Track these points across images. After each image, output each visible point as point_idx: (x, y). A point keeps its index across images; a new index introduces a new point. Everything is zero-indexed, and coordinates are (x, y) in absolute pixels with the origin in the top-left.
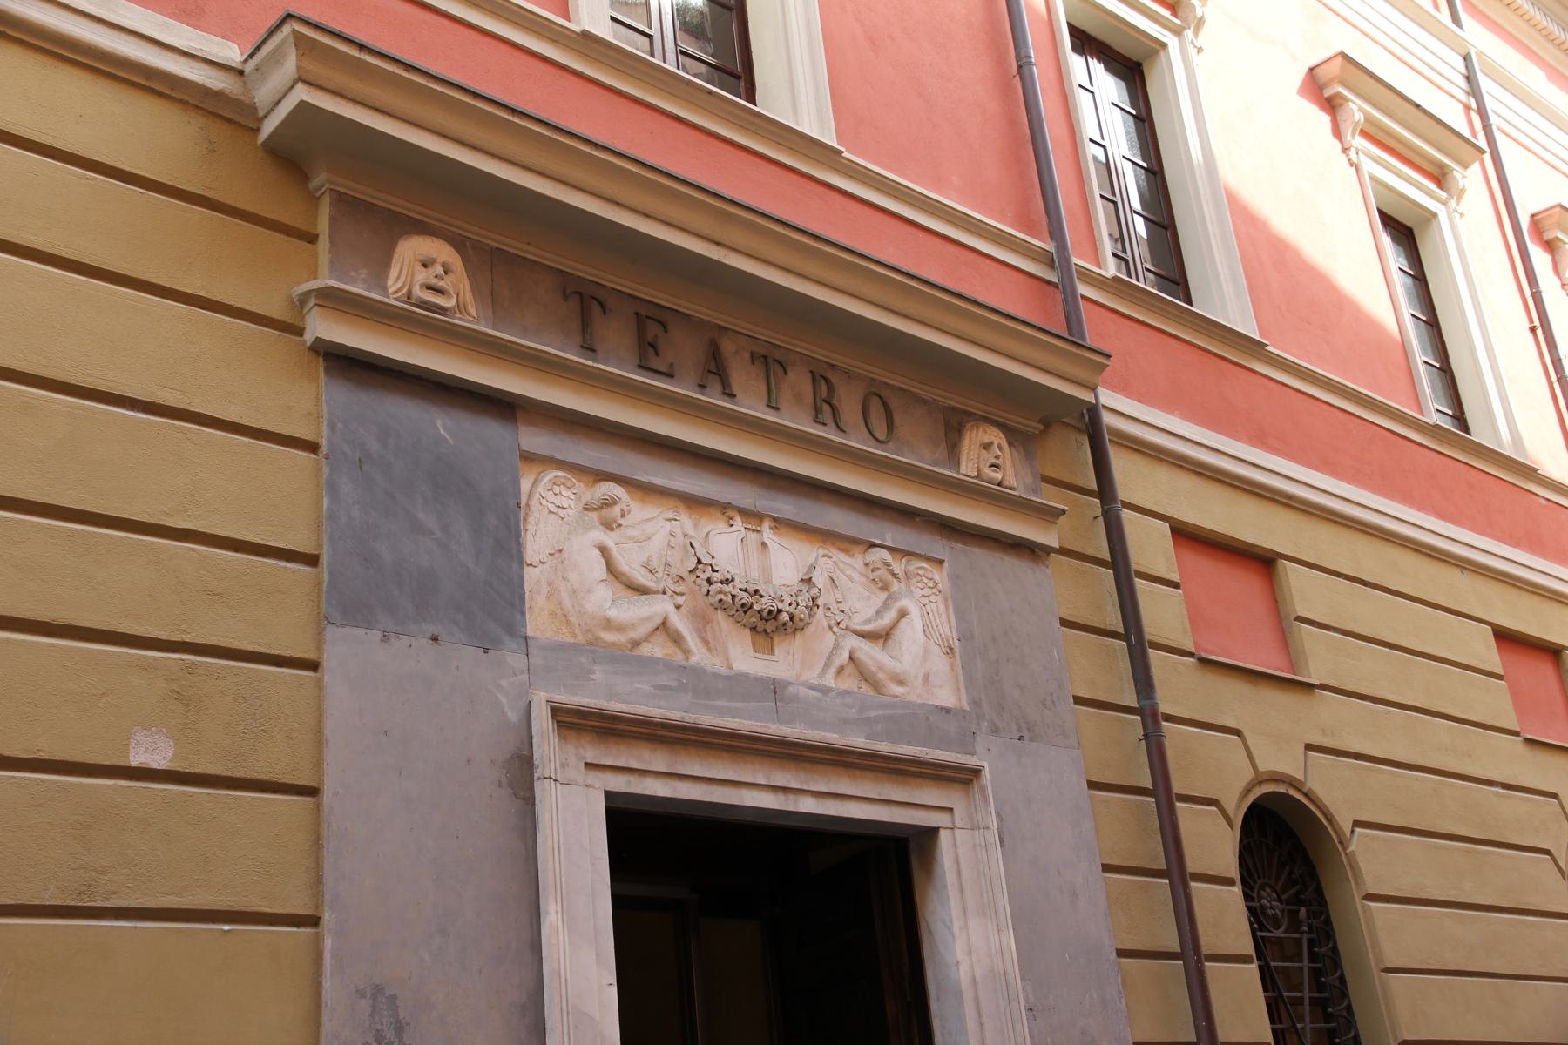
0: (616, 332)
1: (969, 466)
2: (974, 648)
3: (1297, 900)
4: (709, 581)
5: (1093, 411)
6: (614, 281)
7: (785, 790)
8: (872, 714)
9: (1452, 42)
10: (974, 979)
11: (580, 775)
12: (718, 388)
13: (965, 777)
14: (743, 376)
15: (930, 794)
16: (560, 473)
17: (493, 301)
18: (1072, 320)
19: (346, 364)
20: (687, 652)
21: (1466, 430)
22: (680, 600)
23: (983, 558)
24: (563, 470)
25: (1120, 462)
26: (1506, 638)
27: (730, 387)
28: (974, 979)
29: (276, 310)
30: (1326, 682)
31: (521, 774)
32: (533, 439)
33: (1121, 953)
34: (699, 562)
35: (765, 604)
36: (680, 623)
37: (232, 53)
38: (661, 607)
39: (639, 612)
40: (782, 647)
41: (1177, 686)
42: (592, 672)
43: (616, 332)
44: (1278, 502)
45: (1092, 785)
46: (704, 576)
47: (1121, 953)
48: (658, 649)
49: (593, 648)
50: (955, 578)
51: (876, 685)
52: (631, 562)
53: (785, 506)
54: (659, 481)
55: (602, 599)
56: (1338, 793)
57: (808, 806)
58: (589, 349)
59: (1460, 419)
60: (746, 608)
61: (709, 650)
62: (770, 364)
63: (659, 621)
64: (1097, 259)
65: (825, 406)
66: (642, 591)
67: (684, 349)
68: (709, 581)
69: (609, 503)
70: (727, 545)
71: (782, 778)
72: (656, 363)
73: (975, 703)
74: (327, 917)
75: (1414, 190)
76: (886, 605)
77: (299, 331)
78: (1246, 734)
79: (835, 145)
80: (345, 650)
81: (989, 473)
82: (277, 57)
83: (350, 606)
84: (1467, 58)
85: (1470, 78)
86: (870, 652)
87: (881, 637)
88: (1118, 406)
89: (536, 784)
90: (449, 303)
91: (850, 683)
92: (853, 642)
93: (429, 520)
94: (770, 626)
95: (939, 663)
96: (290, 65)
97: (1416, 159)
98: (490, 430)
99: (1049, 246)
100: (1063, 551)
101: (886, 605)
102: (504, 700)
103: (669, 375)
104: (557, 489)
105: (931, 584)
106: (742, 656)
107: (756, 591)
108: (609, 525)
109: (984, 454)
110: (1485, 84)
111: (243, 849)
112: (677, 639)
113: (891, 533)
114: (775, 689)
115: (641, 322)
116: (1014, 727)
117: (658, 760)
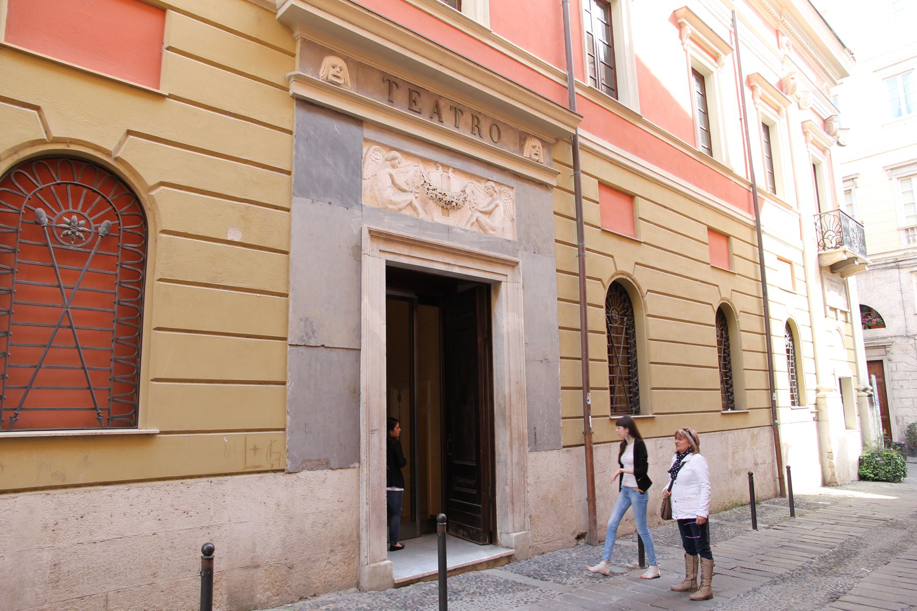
0: (401, 96)
2: (521, 220)
7: (449, 264)
11: (377, 253)
13: (513, 265)
14: (447, 115)
17: (357, 81)
18: (571, 102)
19: (304, 103)
20: (418, 214)
21: (711, 155)
32: (368, 133)
36: (416, 203)
38: (410, 197)
40: (453, 214)
41: (592, 238)
45: (558, 271)
48: (408, 212)
49: (384, 210)
50: (517, 194)
52: (400, 181)
54: (412, 152)
55: (390, 193)
56: (643, 280)
57: (457, 270)
58: (391, 101)
59: (710, 150)
62: (457, 111)
65: (476, 128)
66: (404, 191)
69: (394, 159)
70: (436, 177)
73: (520, 239)
76: (491, 203)
80: (299, 205)
83: (301, 190)
84: (733, 12)
86: (483, 218)
87: (488, 213)
88: (585, 135)
91: (475, 229)
92: (478, 214)
93: (329, 160)
94: (449, 207)
95: (508, 224)
98: (353, 129)
99: (566, 73)
101: (491, 203)
106: (437, 216)
108: (393, 167)
109: (533, 149)
111: (262, 270)
112: (415, 209)
113: (496, 176)
114: (448, 229)
115: (411, 92)
117: (405, 250)
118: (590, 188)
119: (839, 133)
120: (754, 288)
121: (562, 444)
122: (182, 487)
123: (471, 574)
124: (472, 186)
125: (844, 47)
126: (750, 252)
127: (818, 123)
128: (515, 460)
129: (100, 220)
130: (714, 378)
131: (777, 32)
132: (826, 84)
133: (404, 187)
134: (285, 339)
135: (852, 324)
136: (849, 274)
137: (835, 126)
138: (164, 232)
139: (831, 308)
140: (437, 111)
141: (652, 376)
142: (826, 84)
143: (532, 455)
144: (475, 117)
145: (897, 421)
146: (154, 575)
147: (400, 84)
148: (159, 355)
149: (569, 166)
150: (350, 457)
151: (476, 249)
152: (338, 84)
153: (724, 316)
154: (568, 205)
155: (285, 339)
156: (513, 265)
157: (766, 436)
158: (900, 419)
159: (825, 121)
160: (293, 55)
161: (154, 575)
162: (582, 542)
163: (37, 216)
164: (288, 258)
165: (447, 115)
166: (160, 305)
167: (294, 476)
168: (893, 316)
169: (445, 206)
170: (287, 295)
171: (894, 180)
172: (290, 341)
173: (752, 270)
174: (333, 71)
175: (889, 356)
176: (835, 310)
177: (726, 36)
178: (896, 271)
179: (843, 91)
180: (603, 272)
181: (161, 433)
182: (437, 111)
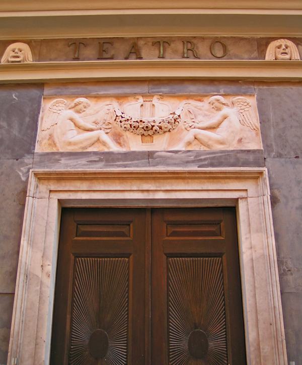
1: (269, 56)
4: (121, 122)
7: (148, 191)
8: (203, 157)
10: (252, 260)
12: (134, 56)
16: (55, 100)
20: (109, 148)
22: (108, 131)
24: (54, 98)
27: (140, 55)
28: (252, 260)
34: (117, 116)
42: (60, 160)
43: (90, 51)
46: (119, 121)
52: (82, 122)
53: (127, 89)
60: (136, 128)
61: (121, 146)
62: (161, 44)
63: (96, 139)
68: (121, 122)
70: (133, 109)
71: (146, 186)
72: (105, 56)
73: (267, 146)
81: (280, 56)
89: (27, 198)
94: (150, 132)
102: (21, 174)
103: (112, 58)
104: (57, 105)
105: (246, 104)
107: (141, 121)
112: (104, 144)
114: (150, 155)
116: (292, 153)
117: (84, 186)
164: (241, 198)
169: (146, 133)
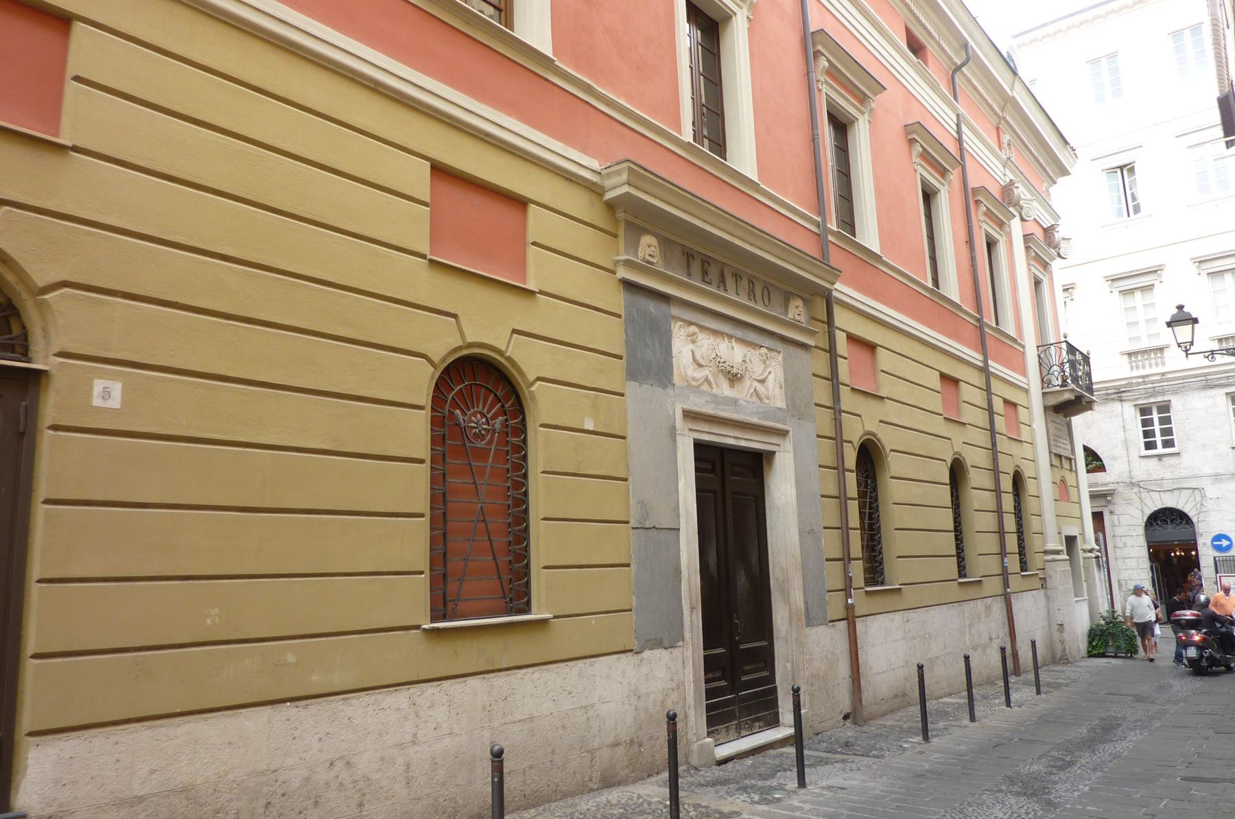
0: (696, 268)
2: (791, 385)
3: (867, 477)
5: (830, 291)
6: (715, 256)
9: (953, 108)
11: (687, 432)
13: (783, 434)
14: (730, 281)
15: (774, 440)
17: (666, 258)
18: (824, 252)
19: (628, 285)
21: (937, 287)
23: (793, 351)
25: (994, 382)
26: (440, 171)
29: (610, 267)
30: (81, 144)
31: (673, 431)
32: (675, 311)
33: (822, 496)
35: (735, 371)
36: (710, 378)
37: (595, 165)
38: (705, 372)
39: (700, 374)
40: (738, 386)
41: (848, 401)
44: (439, 120)
45: (818, 436)
47: (822, 496)
48: (705, 387)
49: (693, 388)
50: (784, 358)
51: (761, 399)
53: (739, 333)
54: (707, 325)
55: (692, 372)
56: (888, 439)
57: (743, 444)
58: (689, 275)
59: (936, 282)
62: (737, 276)
64: (678, 127)
65: (751, 294)
66: (700, 366)
67: (744, 283)
69: (694, 334)
71: (737, 434)
74: (630, 479)
75: (847, 105)
76: (765, 370)
77: (614, 273)
78: (461, 318)
79: (755, 179)
80: (631, 388)
82: (618, 173)
83: (632, 375)
84: (958, 116)
85: (958, 125)
86: (760, 388)
87: (762, 381)
88: (843, 290)
90: (654, 261)
91: (755, 399)
92: (756, 384)
93: (649, 342)
95: (777, 391)
96: (625, 177)
97: (856, 91)
98: (663, 307)
99: (819, 219)
100: (816, 347)
101: (765, 370)
106: (725, 390)
108: (693, 342)
109: (796, 311)
110: (964, 128)
111: (602, 456)
112: (710, 384)
113: (767, 342)
114: (735, 402)
115: (703, 262)
118: (841, 338)
119: (1063, 245)
120: (983, 438)
121: (829, 619)
122: (568, 669)
123: (772, 752)
124: (754, 356)
125: (1066, 143)
126: (978, 397)
127: (1039, 234)
128: (794, 636)
129: (495, 417)
130: (947, 543)
131: (998, 129)
132: (1045, 185)
133: (702, 361)
134: (627, 522)
135: (1076, 472)
136: (1074, 414)
137: (1058, 236)
138: (543, 425)
139: (1056, 455)
140: (722, 281)
141: (895, 544)
142: (1045, 185)
143: (808, 631)
144: (751, 282)
145: (1120, 585)
146: (553, 752)
147: (695, 255)
148: (545, 544)
149: (823, 322)
150: (667, 639)
151: (755, 420)
152: (651, 263)
153: (957, 472)
154: (820, 363)
155: (627, 522)
156: (783, 434)
157: (998, 607)
158: (1123, 582)
159: (1045, 230)
160: (616, 236)
161: (553, 752)
162: (848, 723)
163: (457, 418)
165: (730, 281)
166: (543, 496)
167: (640, 656)
168: (1114, 458)
170: (626, 480)
171: (1116, 292)
172: (633, 523)
173: (981, 418)
174: (648, 251)
175: (1111, 507)
176: (1060, 456)
177: (952, 147)
178: (1118, 404)
179: (1061, 193)
180: (854, 432)
181: (555, 617)
182: (722, 281)
